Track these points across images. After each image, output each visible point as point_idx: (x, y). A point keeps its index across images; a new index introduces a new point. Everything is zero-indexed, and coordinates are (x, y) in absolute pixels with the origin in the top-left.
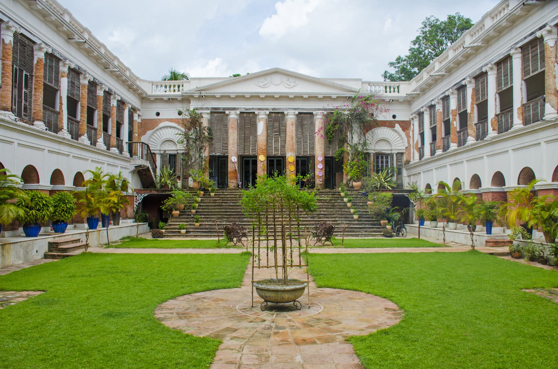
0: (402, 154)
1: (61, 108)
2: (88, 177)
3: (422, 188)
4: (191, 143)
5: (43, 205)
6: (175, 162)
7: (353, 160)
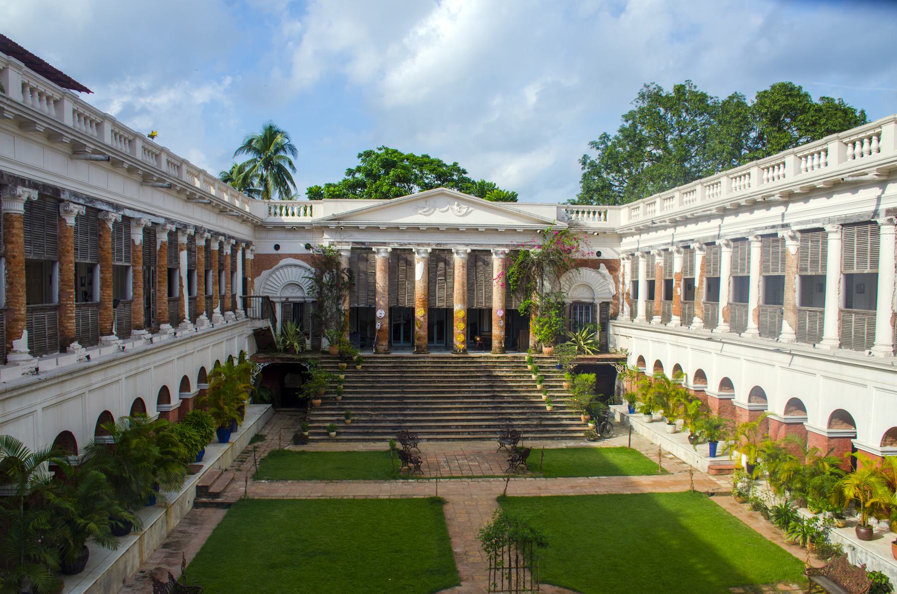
0: (608, 304)
1: (181, 292)
2: (209, 369)
4: (326, 292)
5: (192, 445)
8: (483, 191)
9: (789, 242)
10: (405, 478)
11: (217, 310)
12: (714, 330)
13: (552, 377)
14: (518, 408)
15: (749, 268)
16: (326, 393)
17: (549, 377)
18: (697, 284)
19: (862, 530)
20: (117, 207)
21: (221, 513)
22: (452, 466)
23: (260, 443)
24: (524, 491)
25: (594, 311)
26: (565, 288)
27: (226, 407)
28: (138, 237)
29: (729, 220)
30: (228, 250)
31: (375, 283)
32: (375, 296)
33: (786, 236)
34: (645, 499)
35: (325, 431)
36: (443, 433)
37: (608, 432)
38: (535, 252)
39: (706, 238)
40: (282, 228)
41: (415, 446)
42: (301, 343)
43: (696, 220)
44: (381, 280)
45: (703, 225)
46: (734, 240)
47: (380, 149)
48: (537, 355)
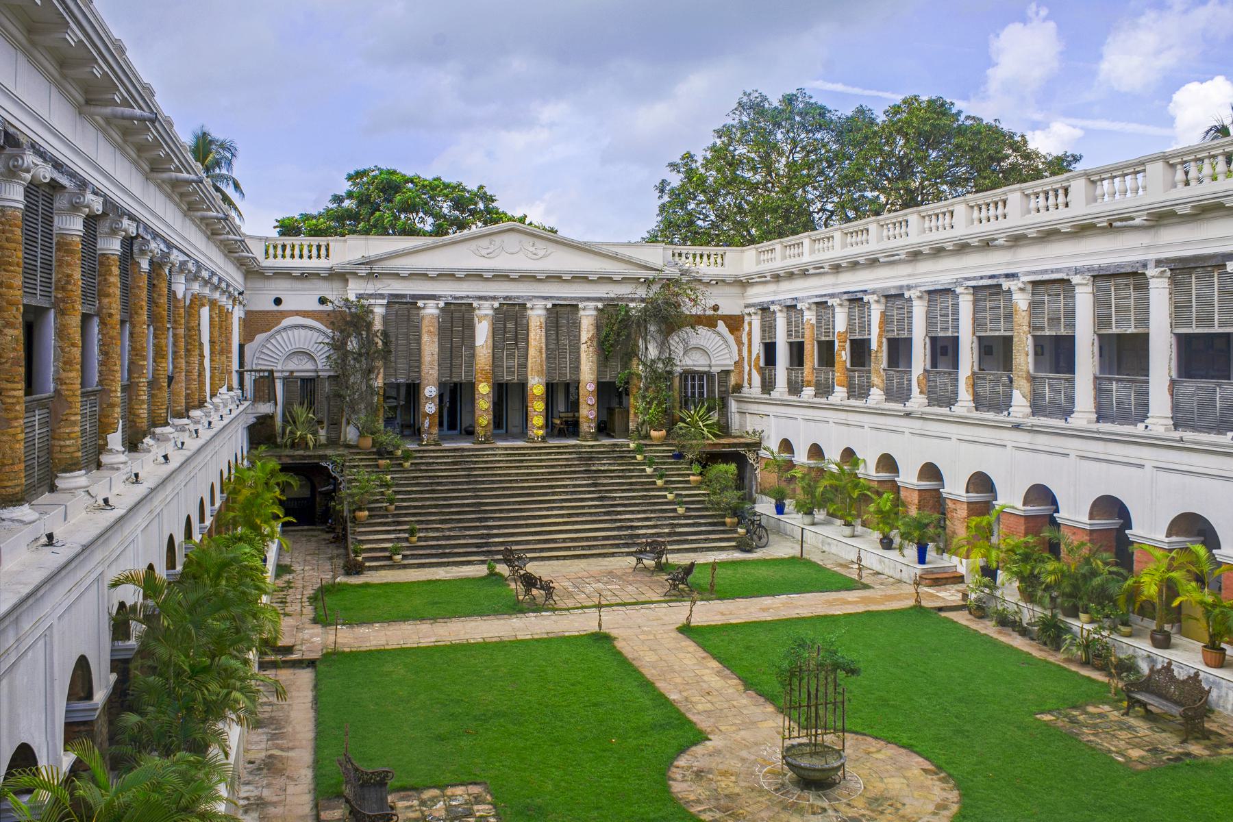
0: (727, 372)
3: (773, 444)
7: (647, 389)
14: (639, 512)
15: (910, 325)
18: (874, 346)
19: (1158, 636)
22: (587, 591)
33: (1013, 288)
35: (387, 554)
46: (930, 292)
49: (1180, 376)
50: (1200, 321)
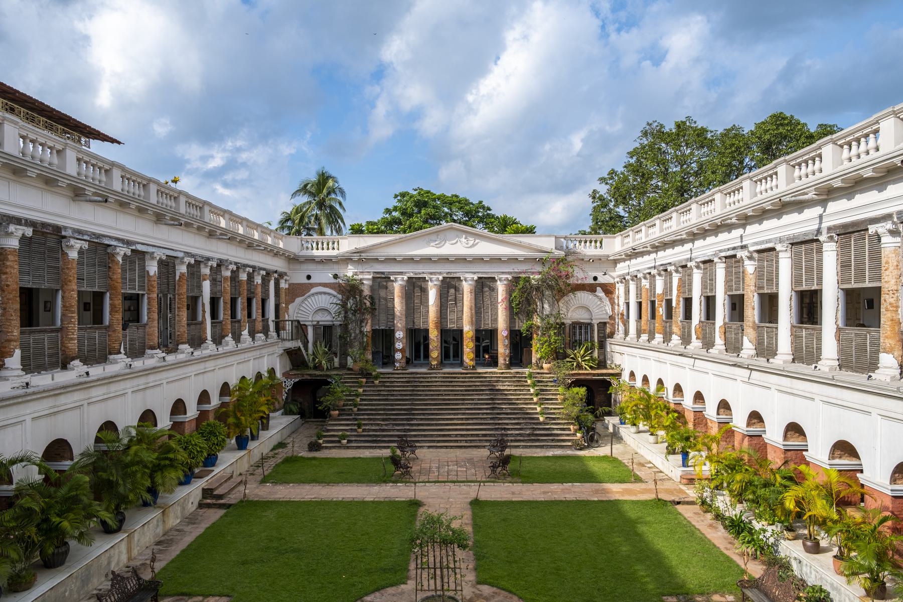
0: (605, 323)
1: (204, 316)
4: (350, 316)
5: (198, 451)
6: (331, 335)
8: (505, 225)
9: (747, 262)
10: (395, 482)
11: (245, 333)
12: (688, 347)
13: (550, 390)
14: (514, 419)
16: (344, 405)
17: (547, 390)
18: (674, 304)
19: (809, 543)
20: (128, 243)
21: (222, 512)
22: (441, 471)
23: (280, 450)
24: (499, 496)
25: (592, 330)
26: (563, 310)
27: (243, 418)
28: (153, 268)
29: (699, 243)
30: (258, 280)
31: (394, 307)
32: (393, 319)
34: (614, 505)
35: (337, 439)
36: (443, 441)
37: (597, 441)
38: (535, 278)
39: (680, 261)
40: (312, 260)
41: (413, 452)
42: (330, 361)
43: (673, 244)
44: (398, 305)
45: (678, 249)
46: (704, 262)
47: (416, 190)
48: (538, 371)
49: (761, 321)
50: (871, 280)
